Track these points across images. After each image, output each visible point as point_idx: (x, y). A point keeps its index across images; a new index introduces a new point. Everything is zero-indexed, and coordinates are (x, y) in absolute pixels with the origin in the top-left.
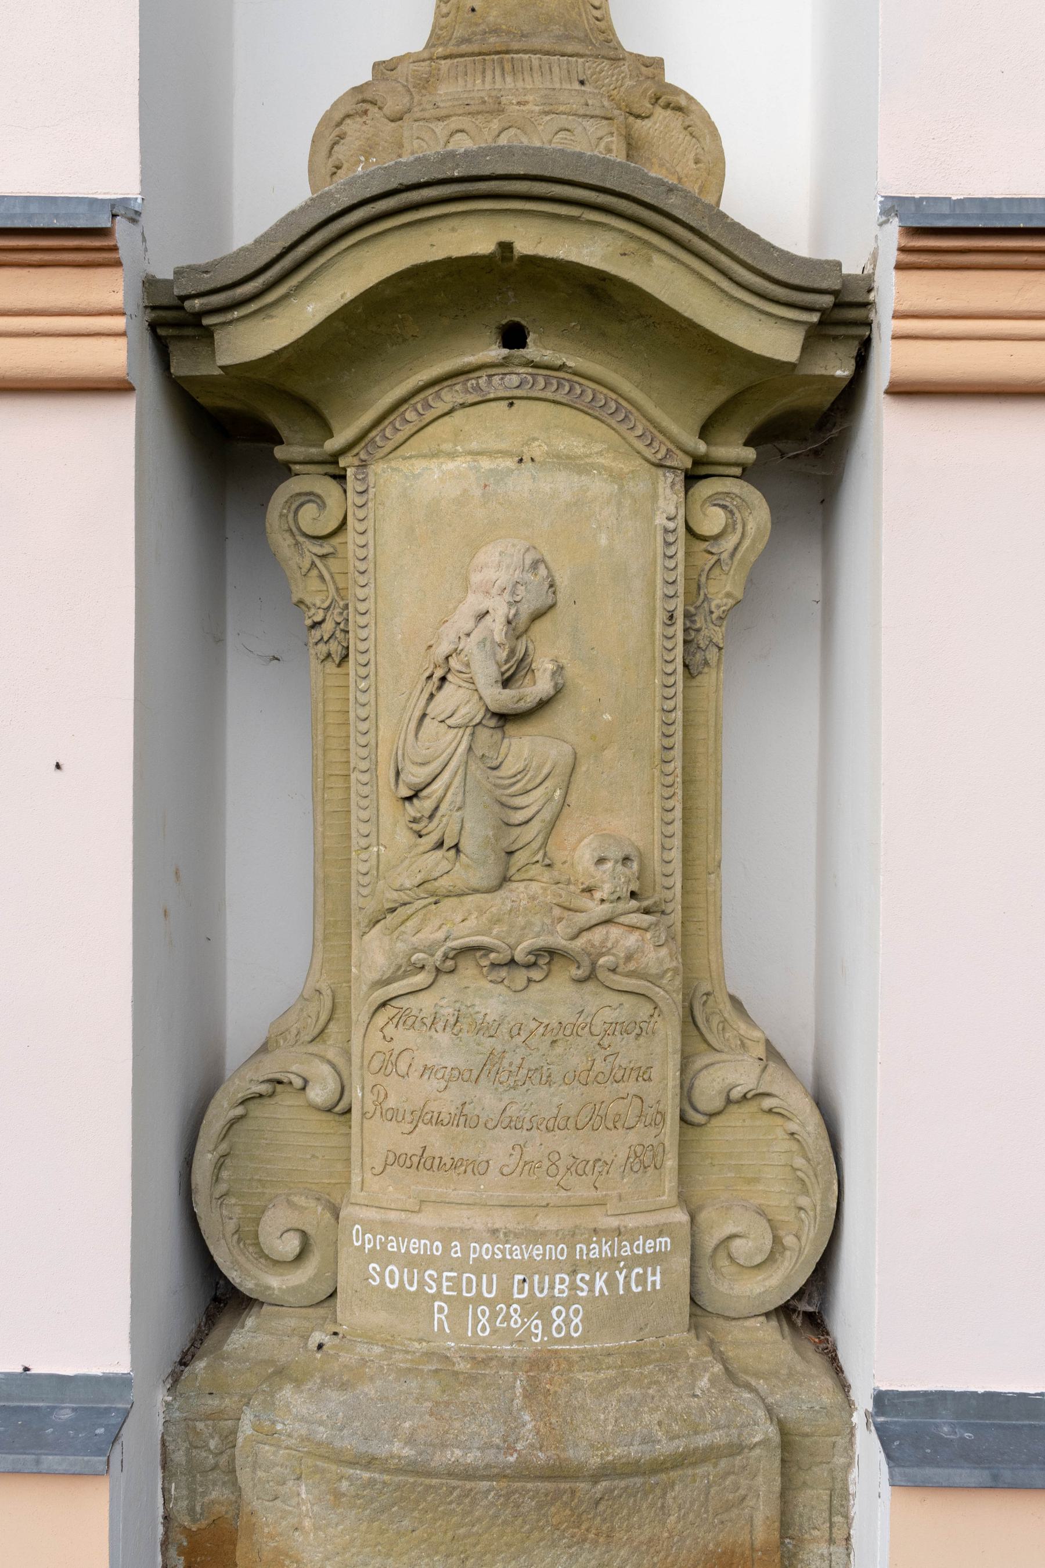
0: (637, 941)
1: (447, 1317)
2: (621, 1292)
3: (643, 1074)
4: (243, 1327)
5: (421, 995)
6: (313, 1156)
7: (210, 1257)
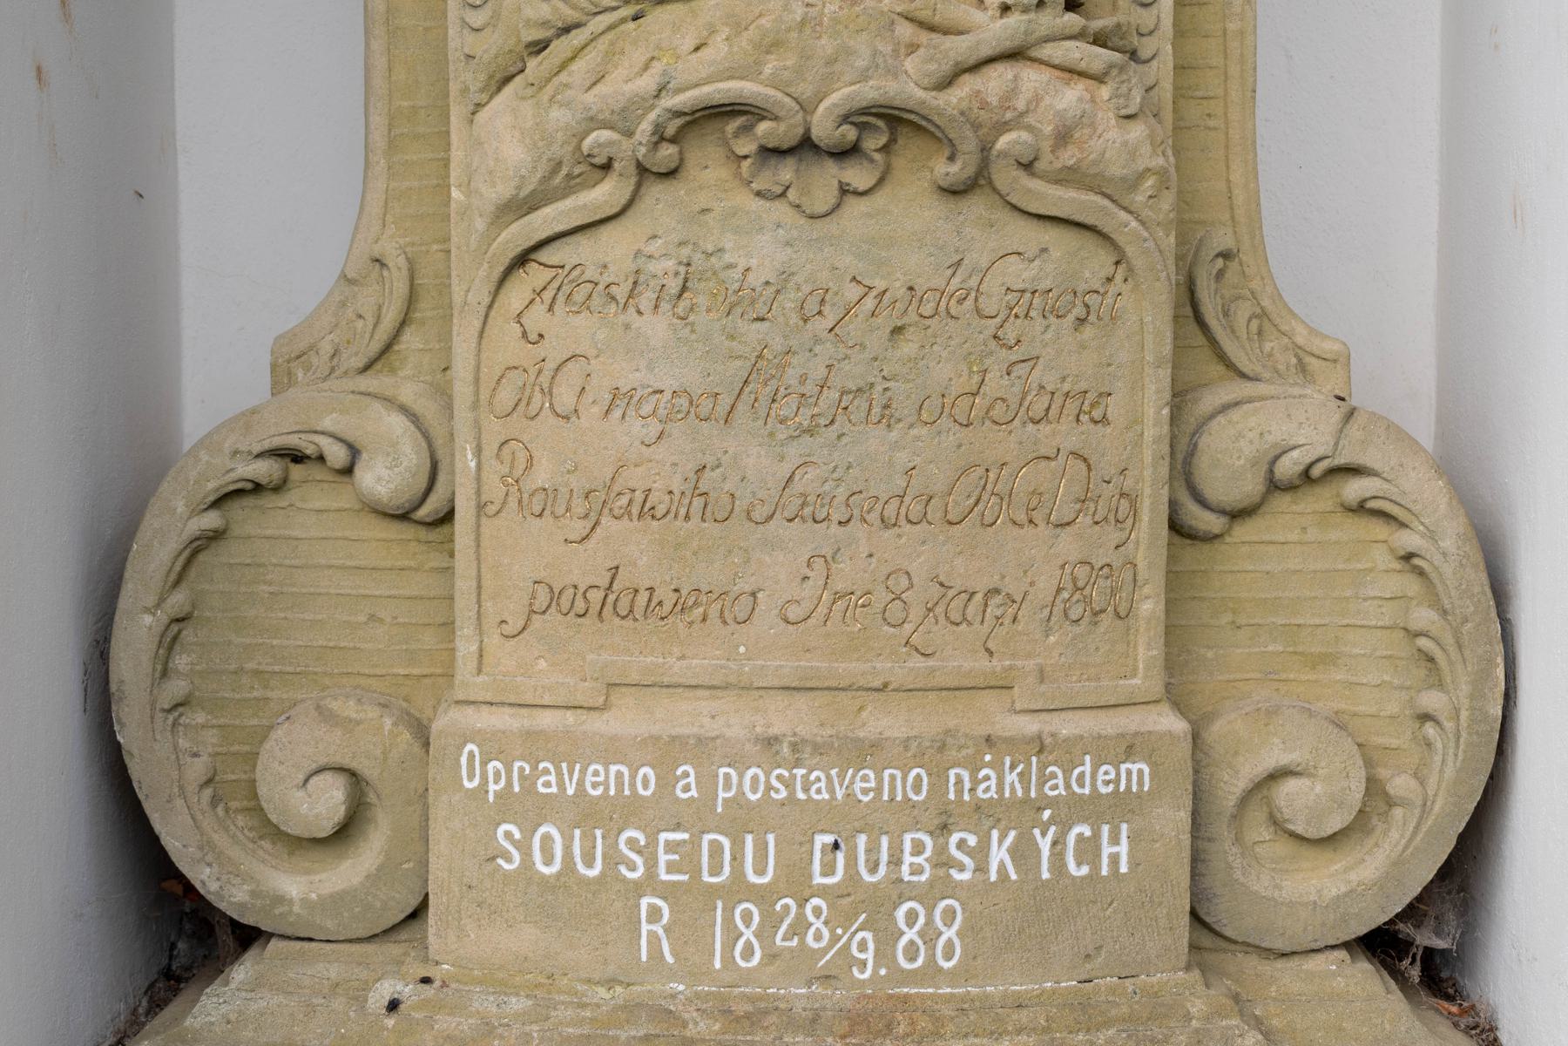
0: (1080, 99)
1: (667, 930)
2: (1046, 875)
3: (1090, 406)
4: (227, 983)
5: (606, 232)
6: (372, 617)
7: (155, 839)
